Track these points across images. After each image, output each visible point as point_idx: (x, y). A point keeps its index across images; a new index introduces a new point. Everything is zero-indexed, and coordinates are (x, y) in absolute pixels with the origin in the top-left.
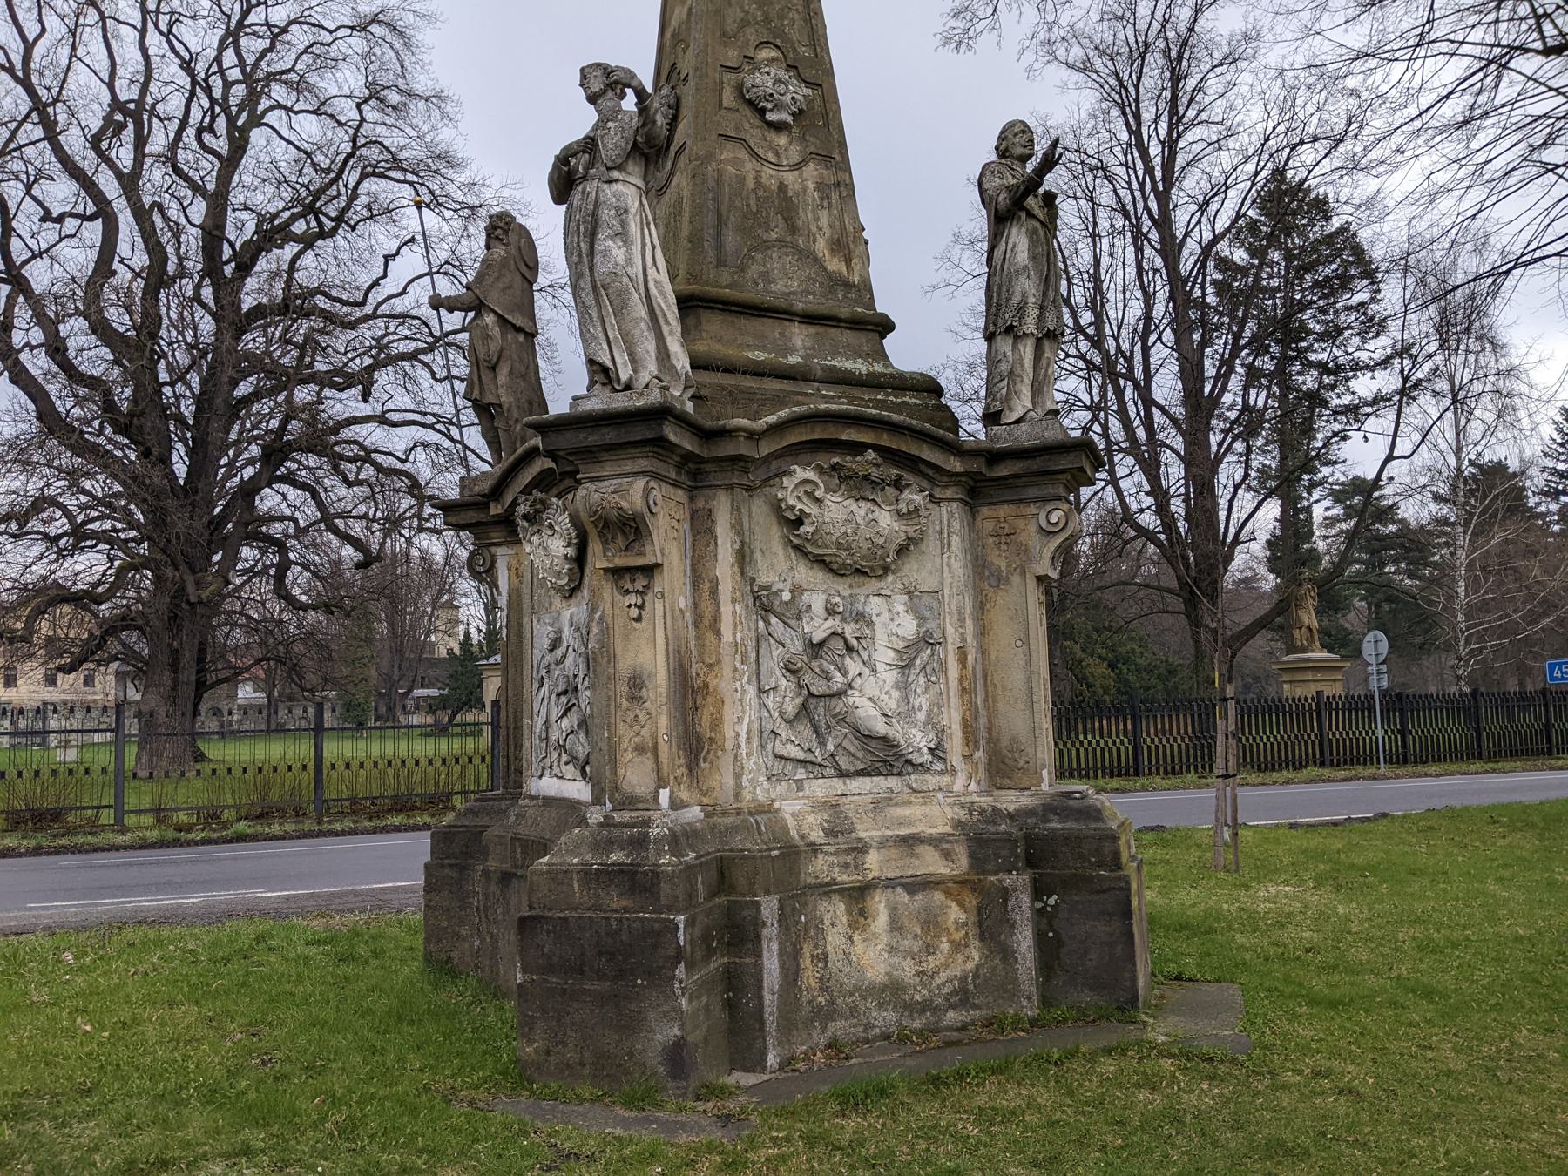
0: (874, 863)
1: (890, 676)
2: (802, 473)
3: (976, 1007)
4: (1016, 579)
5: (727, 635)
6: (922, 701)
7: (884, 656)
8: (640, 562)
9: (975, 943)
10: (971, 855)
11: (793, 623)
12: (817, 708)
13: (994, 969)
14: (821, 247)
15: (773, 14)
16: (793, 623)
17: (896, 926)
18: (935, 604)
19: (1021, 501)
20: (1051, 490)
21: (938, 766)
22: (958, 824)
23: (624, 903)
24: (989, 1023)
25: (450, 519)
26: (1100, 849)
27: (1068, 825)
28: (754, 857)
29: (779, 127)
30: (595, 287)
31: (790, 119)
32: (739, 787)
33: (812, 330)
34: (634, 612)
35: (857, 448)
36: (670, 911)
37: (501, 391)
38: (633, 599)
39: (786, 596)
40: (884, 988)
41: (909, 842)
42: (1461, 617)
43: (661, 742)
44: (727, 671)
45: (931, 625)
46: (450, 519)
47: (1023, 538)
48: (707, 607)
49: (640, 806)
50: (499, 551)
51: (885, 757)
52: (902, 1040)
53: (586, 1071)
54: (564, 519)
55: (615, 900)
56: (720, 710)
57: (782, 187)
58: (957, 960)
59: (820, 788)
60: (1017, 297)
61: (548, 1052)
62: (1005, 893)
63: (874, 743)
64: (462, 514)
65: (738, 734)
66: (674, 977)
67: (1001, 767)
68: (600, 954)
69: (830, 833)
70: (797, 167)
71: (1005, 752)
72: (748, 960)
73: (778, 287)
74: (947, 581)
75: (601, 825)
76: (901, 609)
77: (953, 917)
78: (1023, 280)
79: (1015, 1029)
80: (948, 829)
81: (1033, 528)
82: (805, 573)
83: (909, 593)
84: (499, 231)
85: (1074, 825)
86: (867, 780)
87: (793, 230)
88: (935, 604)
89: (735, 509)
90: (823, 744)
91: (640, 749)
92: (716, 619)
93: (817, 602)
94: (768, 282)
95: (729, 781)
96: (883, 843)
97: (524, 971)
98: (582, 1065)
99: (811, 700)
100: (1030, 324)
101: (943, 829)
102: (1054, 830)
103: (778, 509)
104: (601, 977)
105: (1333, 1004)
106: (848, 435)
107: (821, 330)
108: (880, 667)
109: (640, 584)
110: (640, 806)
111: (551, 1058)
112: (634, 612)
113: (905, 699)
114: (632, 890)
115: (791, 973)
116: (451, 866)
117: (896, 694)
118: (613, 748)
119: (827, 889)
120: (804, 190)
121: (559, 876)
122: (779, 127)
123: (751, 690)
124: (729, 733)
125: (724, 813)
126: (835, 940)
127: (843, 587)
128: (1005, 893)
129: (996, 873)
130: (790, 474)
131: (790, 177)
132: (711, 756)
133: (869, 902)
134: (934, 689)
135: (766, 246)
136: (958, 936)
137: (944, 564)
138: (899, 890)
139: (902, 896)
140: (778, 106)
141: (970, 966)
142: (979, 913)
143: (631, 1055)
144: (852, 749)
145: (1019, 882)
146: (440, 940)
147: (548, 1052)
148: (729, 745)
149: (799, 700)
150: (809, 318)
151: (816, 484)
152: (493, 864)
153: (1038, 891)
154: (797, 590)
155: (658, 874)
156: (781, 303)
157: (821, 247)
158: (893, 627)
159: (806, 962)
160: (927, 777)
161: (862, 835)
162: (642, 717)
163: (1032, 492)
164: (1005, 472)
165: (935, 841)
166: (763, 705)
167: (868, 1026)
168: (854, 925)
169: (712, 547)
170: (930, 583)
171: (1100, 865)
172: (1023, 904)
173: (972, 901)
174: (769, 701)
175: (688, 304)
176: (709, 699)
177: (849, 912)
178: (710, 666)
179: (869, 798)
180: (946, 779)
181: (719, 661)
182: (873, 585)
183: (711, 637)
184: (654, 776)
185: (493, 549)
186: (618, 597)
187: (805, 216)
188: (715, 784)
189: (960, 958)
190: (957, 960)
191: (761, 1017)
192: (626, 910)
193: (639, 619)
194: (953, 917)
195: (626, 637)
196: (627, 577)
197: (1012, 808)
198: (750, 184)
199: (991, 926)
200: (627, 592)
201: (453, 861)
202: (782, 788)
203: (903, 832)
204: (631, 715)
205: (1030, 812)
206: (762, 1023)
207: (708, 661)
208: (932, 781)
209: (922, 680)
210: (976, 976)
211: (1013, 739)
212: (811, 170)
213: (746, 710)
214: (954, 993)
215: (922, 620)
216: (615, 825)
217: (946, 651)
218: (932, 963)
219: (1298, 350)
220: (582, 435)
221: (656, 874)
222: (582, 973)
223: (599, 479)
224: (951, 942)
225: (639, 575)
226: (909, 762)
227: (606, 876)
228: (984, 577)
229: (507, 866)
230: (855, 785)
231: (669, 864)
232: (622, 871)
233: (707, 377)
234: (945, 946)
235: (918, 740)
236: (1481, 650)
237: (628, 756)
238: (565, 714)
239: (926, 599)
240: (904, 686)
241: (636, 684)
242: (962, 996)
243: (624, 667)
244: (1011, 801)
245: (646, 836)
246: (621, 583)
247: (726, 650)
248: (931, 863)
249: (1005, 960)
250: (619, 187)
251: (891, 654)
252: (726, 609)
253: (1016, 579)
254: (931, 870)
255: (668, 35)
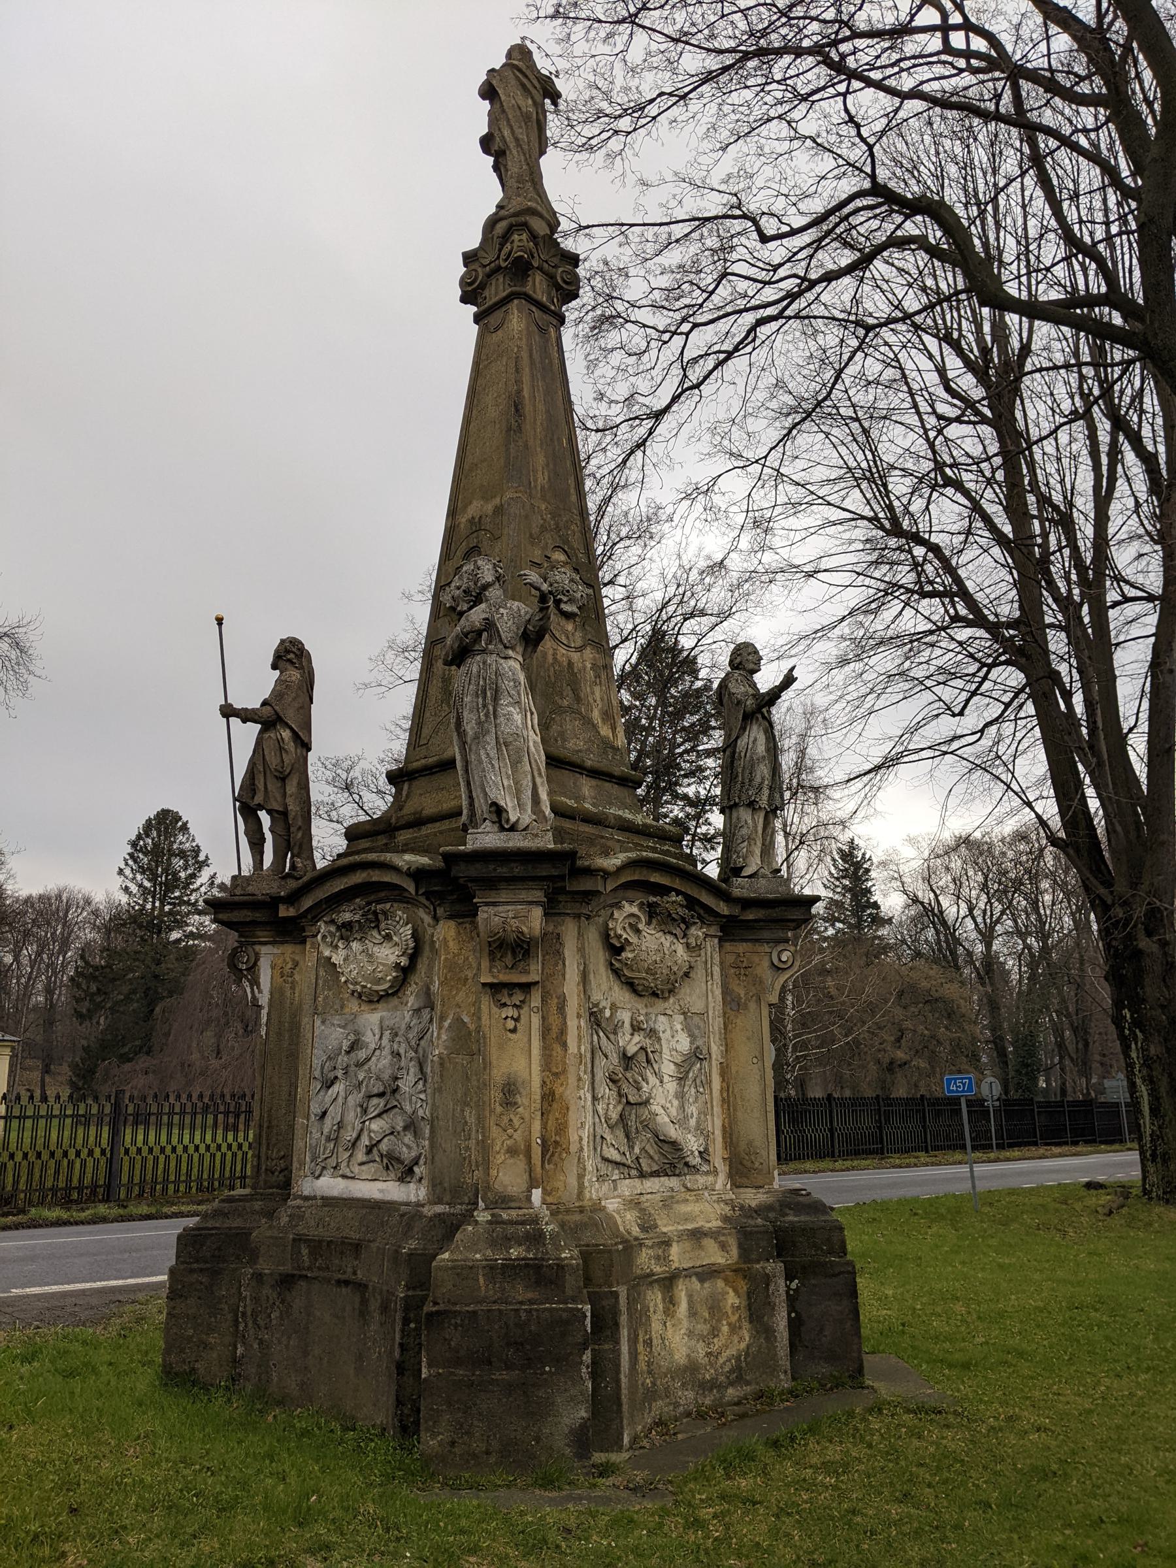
0: (678, 1256)
1: (671, 1086)
2: (631, 909)
3: (748, 1383)
4: (752, 1005)
5: (572, 1047)
6: (693, 1109)
7: (668, 1069)
8: (524, 979)
9: (746, 1325)
10: (740, 1246)
11: (612, 1037)
12: (631, 1116)
13: (760, 1347)
14: (596, 715)
15: (561, 524)
16: (612, 1037)
17: (693, 1313)
18: (702, 1024)
19: (757, 940)
20: (781, 934)
21: (705, 1168)
22: (725, 1219)
23: (530, 1295)
24: (759, 1395)
25: (220, 916)
26: (830, 1237)
27: (803, 1218)
28: (610, 1251)
29: (568, 616)
30: (497, 742)
31: (576, 610)
32: (581, 1187)
33: (594, 782)
34: (510, 1024)
35: (663, 890)
36: (574, 1301)
37: (289, 800)
38: (510, 1012)
39: (608, 1013)
40: (686, 1368)
41: (697, 1235)
42: (789, 1027)
43: (534, 1145)
44: (572, 1080)
45: (699, 1042)
46: (220, 916)
47: (758, 971)
48: (554, 1020)
49: (513, 1205)
50: (264, 950)
51: (672, 1160)
52: (702, 1416)
53: (492, 1460)
54: (408, 931)
55: (521, 1292)
56: (565, 1115)
57: (570, 664)
58: (734, 1342)
59: (629, 1187)
60: (758, 779)
61: (453, 1444)
62: (767, 1279)
63: (666, 1147)
64: (236, 913)
65: (581, 1139)
66: (581, 1363)
67: (741, 1170)
68: (508, 1344)
69: (644, 1229)
70: (580, 649)
71: (743, 1155)
72: (606, 1347)
73: (570, 745)
74: (711, 1005)
75: (490, 1222)
76: (679, 1027)
77: (730, 1302)
78: (762, 767)
79: (782, 1401)
80: (719, 1223)
81: (766, 963)
82: (620, 995)
83: (684, 1013)
84: (291, 656)
85: (808, 1218)
86: (656, 1180)
87: (578, 699)
88: (702, 1024)
89: (580, 935)
90: (631, 1148)
91: (512, 1152)
92: (563, 1031)
93: (625, 1016)
94: (564, 740)
95: (573, 1181)
96: (681, 1235)
97: (430, 1366)
98: (488, 1453)
99: (628, 1108)
100: (763, 801)
101: (716, 1224)
102: (791, 1222)
103: (606, 936)
104: (509, 1367)
105: (966, 1366)
106: (656, 878)
107: (600, 783)
108: (666, 1079)
109: (518, 997)
110: (513, 1205)
111: (456, 1450)
112: (510, 1024)
113: (682, 1107)
114: (538, 1283)
115: (634, 1355)
116: (201, 1270)
117: (676, 1103)
118: (485, 1147)
119: (648, 1279)
120: (584, 668)
121: (464, 1271)
122: (568, 616)
123: (589, 1096)
124: (574, 1137)
125: (568, 1211)
126: (656, 1326)
127: (640, 1005)
128: (767, 1279)
129: (758, 1262)
130: (620, 908)
131: (575, 656)
132: (556, 1158)
133: (676, 1291)
134: (702, 1099)
135: (561, 710)
136: (734, 1319)
137: (704, 994)
138: (694, 1279)
139: (695, 1284)
140: (571, 601)
141: (743, 1345)
142: (749, 1298)
143: (538, 1439)
144: (652, 1152)
145: (775, 1267)
146: (182, 1351)
147: (453, 1444)
148: (573, 1148)
149: (620, 1108)
150: (595, 773)
151: (638, 917)
152: (265, 1266)
153: (789, 1277)
154: (614, 1008)
155: (563, 1267)
156: (575, 758)
157: (596, 715)
158: (673, 1043)
159: (640, 1348)
160: (698, 1177)
161: (665, 1230)
162: (516, 1122)
163: (766, 934)
164: (751, 917)
165: (714, 1234)
166: (595, 1111)
167: (676, 1405)
168: (667, 1312)
169: (560, 967)
170: (698, 1006)
171: (830, 1252)
172: (780, 1286)
173: (743, 1286)
174: (599, 1108)
175: (555, 762)
176: (555, 1105)
177: (664, 1300)
178: (556, 1075)
179: (658, 1197)
180: (711, 1178)
181: (564, 1071)
182: (660, 1005)
183: (558, 1048)
184: (526, 1177)
185: (257, 947)
186: (495, 1010)
187: (586, 689)
188: (560, 1185)
189: (736, 1339)
190: (734, 1342)
191: (619, 1399)
192: (531, 1302)
193: (514, 1031)
194: (730, 1302)
195: (501, 1047)
196: (505, 992)
197: (753, 1204)
198: (550, 659)
199: (757, 1311)
200: (505, 1005)
201: (202, 1266)
202: (605, 1187)
203: (690, 1226)
204: (505, 1119)
205: (769, 1208)
206: (620, 1405)
207: (554, 1070)
208: (701, 1180)
209: (693, 1090)
210: (747, 1354)
211: (750, 1143)
212: (588, 653)
213: (587, 1116)
214: (731, 1371)
215: (692, 1036)
216: (503, 1222)
217: (710, 1065)
218: (718, 1343)
219: (669, 782)
220: (492, 867)
221: (561, 1267)
222: (490, 1363)
223: (494, 904)
224: (729, 1324)
225: (517, 990)
226: (686, 1164)
227: (511, 1270)
228: (732, 1003)
229: (287, 1268)
230: (652, 1184)
231: (572, 1258)
232: (527, 1265)
233: (567, 824)
234: (725, 1329)
235: (692, 1144)
236: (805, 1056)
237: (500, 1158)
238: (379, 1115)
239: (696, 1019)
240: (681, 1096)
241: (510, 1091)
242: (738, 1375)
243: (498, 1074)
244: (753, 1198)
245: (541, 1234)
246: (498, 997)
247: (571, 1061)
248: (714, 1255)
249: (767, 1339)
250: (511, 663)
251: (672, 1067)
252: (572, 1023)
253: (752, 1005)
254: (712, 1260)
255: (463, 520)
